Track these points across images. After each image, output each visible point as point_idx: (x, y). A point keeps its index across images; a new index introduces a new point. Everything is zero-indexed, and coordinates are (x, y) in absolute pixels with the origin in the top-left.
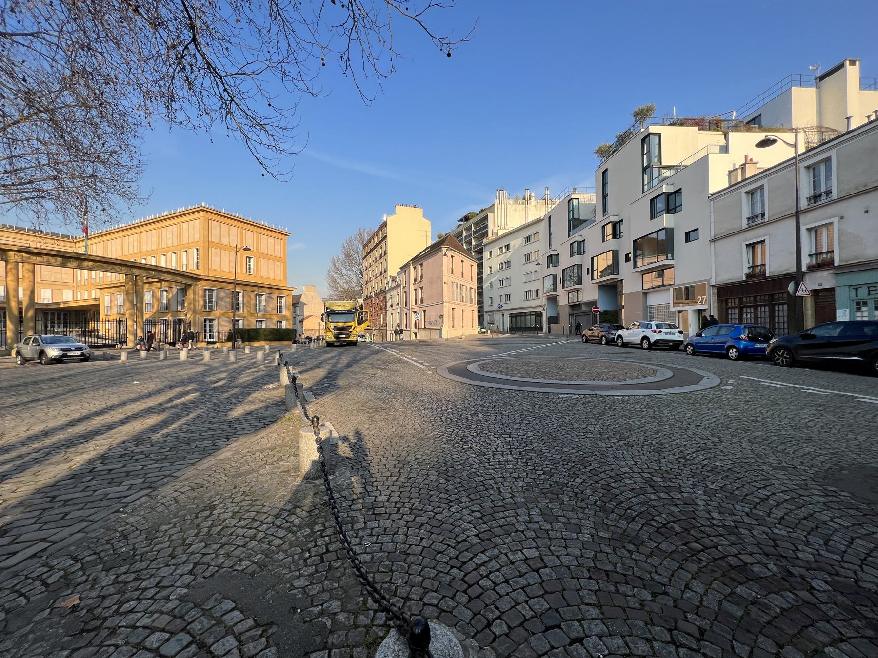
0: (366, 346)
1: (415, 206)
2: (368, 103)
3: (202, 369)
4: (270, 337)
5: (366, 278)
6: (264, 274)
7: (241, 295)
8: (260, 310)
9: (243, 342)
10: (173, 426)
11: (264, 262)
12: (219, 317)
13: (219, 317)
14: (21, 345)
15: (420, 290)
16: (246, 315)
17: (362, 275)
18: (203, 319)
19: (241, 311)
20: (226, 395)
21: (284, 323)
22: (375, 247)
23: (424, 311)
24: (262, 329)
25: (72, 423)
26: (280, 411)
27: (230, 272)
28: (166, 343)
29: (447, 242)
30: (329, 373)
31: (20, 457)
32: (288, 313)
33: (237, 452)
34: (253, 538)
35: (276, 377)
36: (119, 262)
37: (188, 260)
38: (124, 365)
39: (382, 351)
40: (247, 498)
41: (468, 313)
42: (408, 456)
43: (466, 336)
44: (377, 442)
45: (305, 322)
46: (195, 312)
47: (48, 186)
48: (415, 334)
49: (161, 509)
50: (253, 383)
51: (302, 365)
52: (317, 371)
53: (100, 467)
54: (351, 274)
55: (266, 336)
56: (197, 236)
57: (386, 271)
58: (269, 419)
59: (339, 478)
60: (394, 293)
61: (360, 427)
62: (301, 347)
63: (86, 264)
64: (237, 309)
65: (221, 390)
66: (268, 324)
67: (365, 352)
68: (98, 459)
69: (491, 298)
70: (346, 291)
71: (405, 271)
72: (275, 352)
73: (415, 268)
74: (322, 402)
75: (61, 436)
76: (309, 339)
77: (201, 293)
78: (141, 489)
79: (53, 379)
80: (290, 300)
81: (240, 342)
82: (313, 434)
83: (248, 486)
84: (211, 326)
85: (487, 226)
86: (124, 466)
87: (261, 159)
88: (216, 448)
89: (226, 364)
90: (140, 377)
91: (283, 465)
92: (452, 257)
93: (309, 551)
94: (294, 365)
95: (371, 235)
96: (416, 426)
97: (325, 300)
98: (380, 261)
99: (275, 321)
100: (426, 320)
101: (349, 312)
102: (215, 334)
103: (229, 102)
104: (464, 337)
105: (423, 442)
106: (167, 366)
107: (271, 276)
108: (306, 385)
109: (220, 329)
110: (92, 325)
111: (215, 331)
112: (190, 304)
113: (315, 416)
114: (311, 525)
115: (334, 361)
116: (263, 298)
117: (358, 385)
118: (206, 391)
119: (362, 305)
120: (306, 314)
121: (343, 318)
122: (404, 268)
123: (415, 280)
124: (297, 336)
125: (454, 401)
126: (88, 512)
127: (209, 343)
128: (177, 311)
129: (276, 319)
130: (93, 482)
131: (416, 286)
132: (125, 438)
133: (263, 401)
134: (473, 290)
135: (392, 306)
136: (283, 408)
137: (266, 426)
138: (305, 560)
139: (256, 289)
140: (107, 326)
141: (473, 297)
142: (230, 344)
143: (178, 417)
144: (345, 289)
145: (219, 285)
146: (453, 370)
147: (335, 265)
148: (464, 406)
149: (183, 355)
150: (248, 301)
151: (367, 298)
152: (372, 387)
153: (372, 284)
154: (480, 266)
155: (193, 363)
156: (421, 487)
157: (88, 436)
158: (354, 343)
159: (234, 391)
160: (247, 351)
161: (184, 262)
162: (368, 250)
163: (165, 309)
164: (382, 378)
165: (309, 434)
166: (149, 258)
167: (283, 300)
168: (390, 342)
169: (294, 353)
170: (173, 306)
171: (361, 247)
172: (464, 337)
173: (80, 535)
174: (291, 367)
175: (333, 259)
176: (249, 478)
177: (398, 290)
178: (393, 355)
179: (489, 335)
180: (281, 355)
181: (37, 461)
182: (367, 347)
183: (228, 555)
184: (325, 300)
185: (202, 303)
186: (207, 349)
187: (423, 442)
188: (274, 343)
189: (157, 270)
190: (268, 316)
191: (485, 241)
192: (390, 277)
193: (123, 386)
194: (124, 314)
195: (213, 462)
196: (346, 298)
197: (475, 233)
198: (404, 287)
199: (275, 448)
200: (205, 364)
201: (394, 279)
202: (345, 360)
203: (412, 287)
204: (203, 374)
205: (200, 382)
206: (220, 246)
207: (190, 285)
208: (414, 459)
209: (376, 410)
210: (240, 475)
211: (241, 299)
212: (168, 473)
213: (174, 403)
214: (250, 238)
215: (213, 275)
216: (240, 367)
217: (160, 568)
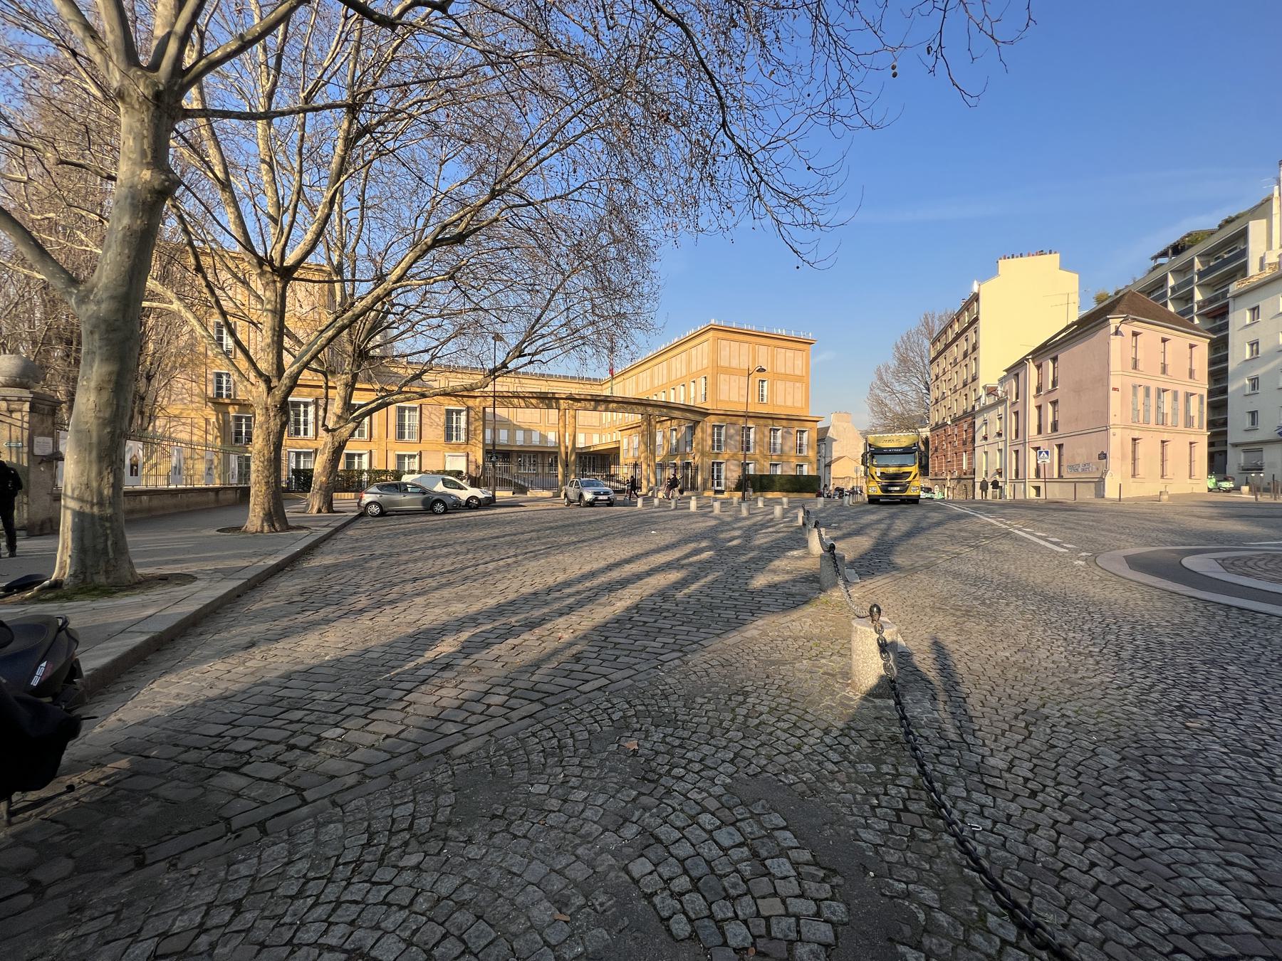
0: (938, 507)
1: (1041, 253)
2: (972, 101)
3: (713, 523)
4: (787, 487)
5: (935, 393)
6: (780, 400)
7: (752, 430)
8: (774, 451)
9: (754, 492)
10: (693, 587)
11: (780, 385)
12: (728, 460)
13: (728, 460)
14: (567, 487)
15: (1050, 407)
16: (758, 457)
17: (928, 390)
19: (752, 451)
20: (743, 558)
21: (805, 468)
22: (955, 340)
23: (1060, 446)
24: (776, 475)
25: (610, 568)
26: (812, 588)
27: (739, 402)
29: (1122, 306)
30: (878, 544)
31: (578, 592)
32: (811, 453)
33: (764, 634)
34: (798, 749)
35: (803, 543)
37: (696, 393)
38: (640, 513)
39: (967, 516)
40: (783, 695)
41: (1178, 446)
42: (1044, 706)
43: (1172, 497)
44: (976, 666)
45: (833, 466)
46: (703, 454)
47: (588, 332)
48: (1038, 489)
49: (693, 677)
50: (772, 547)
51: (835, 528)
52: (858, 539)
53: (636, 617)
54: (909, 391)
55: (782, 485)
56: (705, 362)
57: (974, 379)
58: (798, 598)
59: (918, 709)
60: (992, 415)
61: (941, 636)
62: (829, 503)
63: (611, 405)
64: (748, 449)
65: (736, 551)
66: (785, 468)
67: (936, 516)
68: (634, 608)
69: (1253, 414)
70: (897, 416)
71: (1017, 375)
72: (795, 508)
73: (1039, 367)
74: (871, 586)
75: (603, 579)
76: (840, 491)
77: (709, 431)
78: (673, 651)
79: (590, 522)
80: (814, 435)
81: (750, 492)
82: (873, 630)
83: (783, 679)
84: (719, 471)
85: (1244, 253)
86: (655, 622)
87: (796, 246)
88: (739, 624)
89: (738, 520)
90: (656, 526)
91: (825, 665)
92: (1135, 334)
93: (877, 796)
94: (828, 526)
95: (946, 321)
96: (1056, 657)
97: (865, 434)
98: (963, 363)
99: (793, 465)
100: (1064, 463)
101: (907, 451)
102: (723, 481)
103: (757, 183)
104: (1165, 497)
105: (1076, 689)
106: (677, 518)
107: (789, 403)
108: (848, 557)
109: (729, 475)
110: (613, 470)
111: (723, 477)
112: (698, 444)
113: (875, 605)
114: (878, 762)
115: (883, 526)
116: (779, 433)
117: (929, 567)
118: (723, 552)
119: (927, 439)
120: (835, 455)
121: (898, 460)
122: (1016, 370)
123: (1039, 389)
124: (822, 486)
125: (1151, 627)
126: (633, 661)
127: (717, 492)
128: (685, 454)
129: (795, 462)
130: (634, 632)
131: (1040, 401)
132: (653, 591)
133: (788, 572)
134: (1194, 401)
135: (985, 438)
136: (815, 585)
137: (795, 606)
138: (873, 808)
139: (770, 422)
140: (625, 470)
141: (1194, 411)
142: (740, 494)
143: (696, 578)
144: (896, 414)
145: (728, 419)
146: (1136, 563)
147: (881, 379)
148: (1179, 639)
149: (693, 504)
150: (761, 439)
151: (937, 427)
152: (956, 575)
153: (948, 402)
154: (1219, 349)
155: (704, 515)
156: (1079, 768)
157: (624, 583)
158: (915, 501)
159: (751, 555)
160: (760, 504)
161: (692, 395)
162: (939, 346)
163: (674, 452)
164: (973, 561)
165: (867, 629)
166: (659, 394)
167: (805, 435)
168: (979, 502)
169: (821, 511)
170: (682, 449)
171: (927, 343)
172: (1165, 497)
173: (629, 682)
174: (823, 530)
175: (879, 370)
176: (784, 669)
177: (1001, 409)
178: (992, 524)
179: (1245, 494)
180: (807, 513)
181: (590, 600)
182: (938, 508)
183: (770, 759)
184: (865, 434)
185: (710, 442)
186: (716, 499)
187: (1076, 689)
188: (793, 495)
189: (667, 406)
190: (785, 458)
191: (1234, 287)
192: (984, 387)
193: (643, 535)
194: (639, 458)
195: (739, 638)
196: (899, 428)
197: (1201, 274)
198: (1014, 404)
199: (812, 639)
200: (715, 518)
201: (991, 391)
202: (901, 526)
203: (1032, 403)
204: (714, 529)
205: (713, 539)
206: (729, 371)
207: (699, 422)
208: (1058, 714)
209: (967, 613)
210: (773, 663)
211: (752, 436)
212: (696, 639)
213: (691, 559)
214: (764, 354)
215: (723, 407)
216: (755, 525)
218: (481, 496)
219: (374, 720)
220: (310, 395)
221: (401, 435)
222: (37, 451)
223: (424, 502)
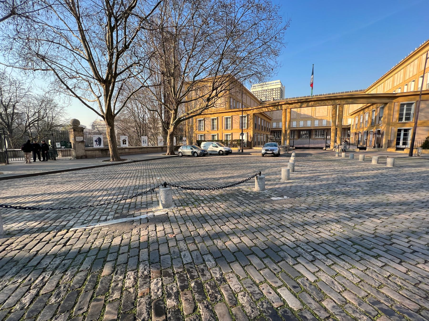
18: (396, 129)
28: (358, 148)
36: (327, 98)
46: (389, 124)
63: (310, 103)
217: (108, 95)
218: (224, 150)
219: (373, 234)
220: (203, 117)
221: (227, 128)
222: (77, 140)
223: (192, 152)
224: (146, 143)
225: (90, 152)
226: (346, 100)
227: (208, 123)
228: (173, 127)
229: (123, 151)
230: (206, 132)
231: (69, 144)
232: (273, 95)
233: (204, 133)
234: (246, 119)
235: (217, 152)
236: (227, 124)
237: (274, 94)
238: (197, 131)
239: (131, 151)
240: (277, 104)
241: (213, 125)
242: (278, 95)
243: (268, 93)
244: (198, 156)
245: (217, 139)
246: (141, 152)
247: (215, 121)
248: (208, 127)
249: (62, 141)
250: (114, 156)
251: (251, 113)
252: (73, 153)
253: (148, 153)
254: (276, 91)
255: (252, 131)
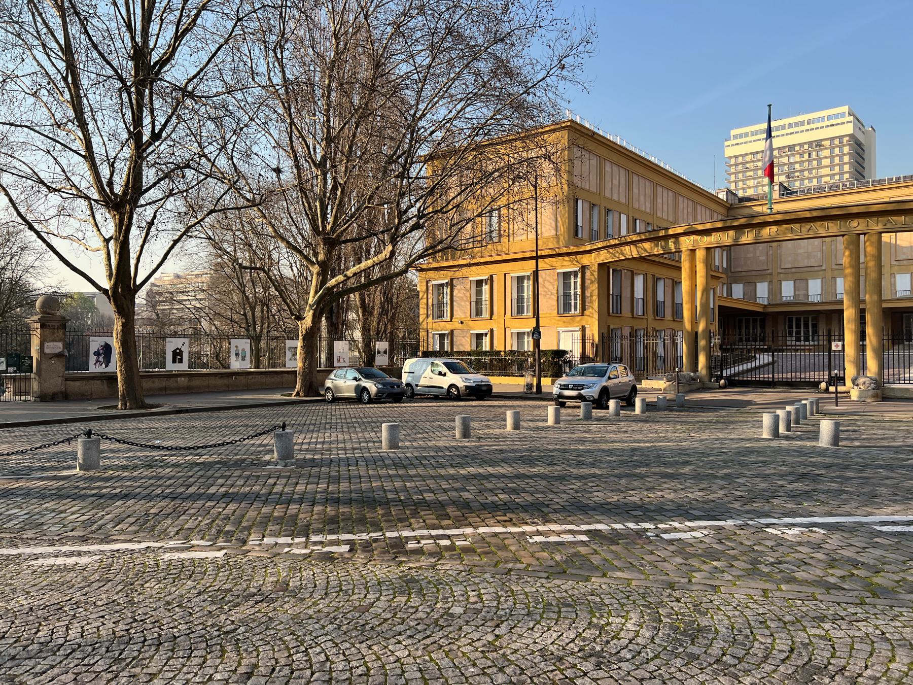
36: (815, 214)
221: (520, 310)
222: (47, 351)
224: (243, 359)
225: (78, 383)
226: (885, 219)
227: (463, 294)
228: (312, 312)
229: (171, 383)
230: (455, 325)
231: (27, 362)
232: (820, 167)
233: (450, 326)
234: (579, 280)
235: (444, 391)
236: (520, 300)
237: (825, 162)
238: (430, 319)
239: (197, 382)
240: (662, 233)
241: (479, 302)
242: (841, 165)
243: (797, 158)
244: (371, 401)
245: (488, 349)
246: (228, 386)
247: (486, 288)
248: (463, 310)
249: (11, 355)
250: (128, 394)
251: (592, 261)
252: (35, 386)
253: (249, 389)
254: (832, 149)
255: (597, 323)
